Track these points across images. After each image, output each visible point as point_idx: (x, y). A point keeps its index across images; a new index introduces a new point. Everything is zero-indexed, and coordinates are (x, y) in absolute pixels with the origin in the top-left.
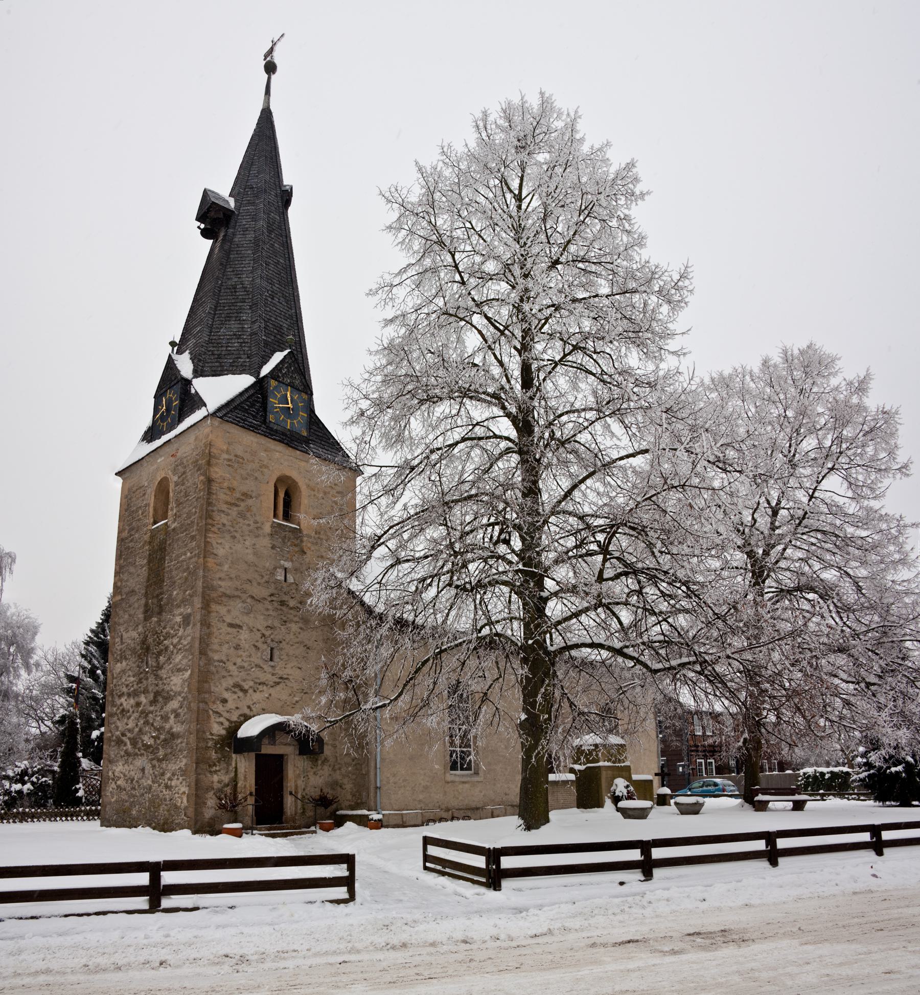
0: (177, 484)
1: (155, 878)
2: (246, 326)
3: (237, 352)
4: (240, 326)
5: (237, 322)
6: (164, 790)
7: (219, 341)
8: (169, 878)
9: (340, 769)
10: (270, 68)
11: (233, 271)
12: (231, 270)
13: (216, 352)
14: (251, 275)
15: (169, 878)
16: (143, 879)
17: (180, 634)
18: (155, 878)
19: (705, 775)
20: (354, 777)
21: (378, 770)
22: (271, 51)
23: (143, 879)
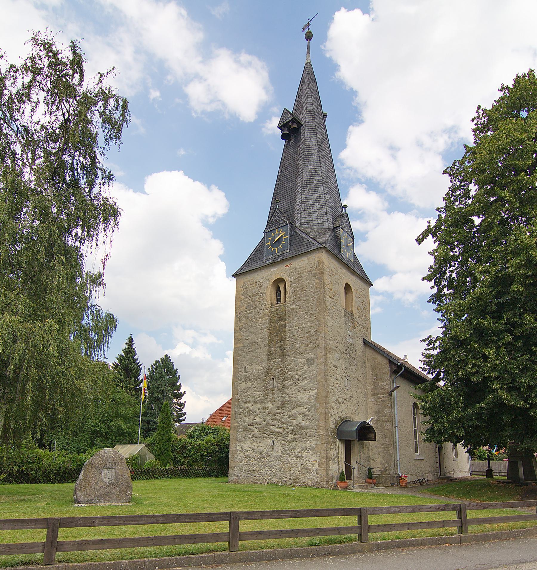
0: (292, 283)
1: (234, 527)
2: (322, 196)
3: (319, 211)
4: (319, 195)
5: (316, 193)
6: (295, 459)
7: (307, 203)
8: (244, 526)
9: (372, 450)
10: (309, 37)
11: (308, 162)
12: (307, 161)
13: (306, 209)
14: (319, 165)
15: (244, 526)
16: (223, 527)
17: (304, 369)
18: (234, 527)
19: (403, 368)
20: (383, 454)
21: (398, 451)
22: (308, 25)
23: (223, 527)
